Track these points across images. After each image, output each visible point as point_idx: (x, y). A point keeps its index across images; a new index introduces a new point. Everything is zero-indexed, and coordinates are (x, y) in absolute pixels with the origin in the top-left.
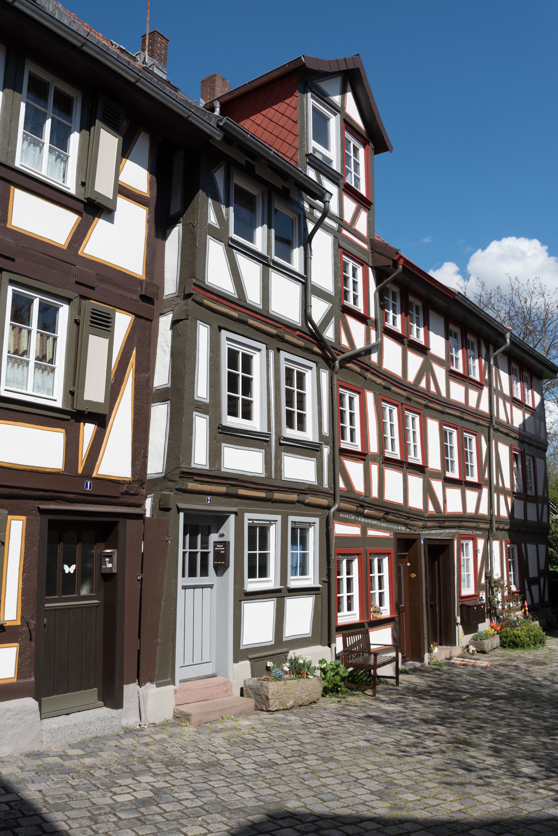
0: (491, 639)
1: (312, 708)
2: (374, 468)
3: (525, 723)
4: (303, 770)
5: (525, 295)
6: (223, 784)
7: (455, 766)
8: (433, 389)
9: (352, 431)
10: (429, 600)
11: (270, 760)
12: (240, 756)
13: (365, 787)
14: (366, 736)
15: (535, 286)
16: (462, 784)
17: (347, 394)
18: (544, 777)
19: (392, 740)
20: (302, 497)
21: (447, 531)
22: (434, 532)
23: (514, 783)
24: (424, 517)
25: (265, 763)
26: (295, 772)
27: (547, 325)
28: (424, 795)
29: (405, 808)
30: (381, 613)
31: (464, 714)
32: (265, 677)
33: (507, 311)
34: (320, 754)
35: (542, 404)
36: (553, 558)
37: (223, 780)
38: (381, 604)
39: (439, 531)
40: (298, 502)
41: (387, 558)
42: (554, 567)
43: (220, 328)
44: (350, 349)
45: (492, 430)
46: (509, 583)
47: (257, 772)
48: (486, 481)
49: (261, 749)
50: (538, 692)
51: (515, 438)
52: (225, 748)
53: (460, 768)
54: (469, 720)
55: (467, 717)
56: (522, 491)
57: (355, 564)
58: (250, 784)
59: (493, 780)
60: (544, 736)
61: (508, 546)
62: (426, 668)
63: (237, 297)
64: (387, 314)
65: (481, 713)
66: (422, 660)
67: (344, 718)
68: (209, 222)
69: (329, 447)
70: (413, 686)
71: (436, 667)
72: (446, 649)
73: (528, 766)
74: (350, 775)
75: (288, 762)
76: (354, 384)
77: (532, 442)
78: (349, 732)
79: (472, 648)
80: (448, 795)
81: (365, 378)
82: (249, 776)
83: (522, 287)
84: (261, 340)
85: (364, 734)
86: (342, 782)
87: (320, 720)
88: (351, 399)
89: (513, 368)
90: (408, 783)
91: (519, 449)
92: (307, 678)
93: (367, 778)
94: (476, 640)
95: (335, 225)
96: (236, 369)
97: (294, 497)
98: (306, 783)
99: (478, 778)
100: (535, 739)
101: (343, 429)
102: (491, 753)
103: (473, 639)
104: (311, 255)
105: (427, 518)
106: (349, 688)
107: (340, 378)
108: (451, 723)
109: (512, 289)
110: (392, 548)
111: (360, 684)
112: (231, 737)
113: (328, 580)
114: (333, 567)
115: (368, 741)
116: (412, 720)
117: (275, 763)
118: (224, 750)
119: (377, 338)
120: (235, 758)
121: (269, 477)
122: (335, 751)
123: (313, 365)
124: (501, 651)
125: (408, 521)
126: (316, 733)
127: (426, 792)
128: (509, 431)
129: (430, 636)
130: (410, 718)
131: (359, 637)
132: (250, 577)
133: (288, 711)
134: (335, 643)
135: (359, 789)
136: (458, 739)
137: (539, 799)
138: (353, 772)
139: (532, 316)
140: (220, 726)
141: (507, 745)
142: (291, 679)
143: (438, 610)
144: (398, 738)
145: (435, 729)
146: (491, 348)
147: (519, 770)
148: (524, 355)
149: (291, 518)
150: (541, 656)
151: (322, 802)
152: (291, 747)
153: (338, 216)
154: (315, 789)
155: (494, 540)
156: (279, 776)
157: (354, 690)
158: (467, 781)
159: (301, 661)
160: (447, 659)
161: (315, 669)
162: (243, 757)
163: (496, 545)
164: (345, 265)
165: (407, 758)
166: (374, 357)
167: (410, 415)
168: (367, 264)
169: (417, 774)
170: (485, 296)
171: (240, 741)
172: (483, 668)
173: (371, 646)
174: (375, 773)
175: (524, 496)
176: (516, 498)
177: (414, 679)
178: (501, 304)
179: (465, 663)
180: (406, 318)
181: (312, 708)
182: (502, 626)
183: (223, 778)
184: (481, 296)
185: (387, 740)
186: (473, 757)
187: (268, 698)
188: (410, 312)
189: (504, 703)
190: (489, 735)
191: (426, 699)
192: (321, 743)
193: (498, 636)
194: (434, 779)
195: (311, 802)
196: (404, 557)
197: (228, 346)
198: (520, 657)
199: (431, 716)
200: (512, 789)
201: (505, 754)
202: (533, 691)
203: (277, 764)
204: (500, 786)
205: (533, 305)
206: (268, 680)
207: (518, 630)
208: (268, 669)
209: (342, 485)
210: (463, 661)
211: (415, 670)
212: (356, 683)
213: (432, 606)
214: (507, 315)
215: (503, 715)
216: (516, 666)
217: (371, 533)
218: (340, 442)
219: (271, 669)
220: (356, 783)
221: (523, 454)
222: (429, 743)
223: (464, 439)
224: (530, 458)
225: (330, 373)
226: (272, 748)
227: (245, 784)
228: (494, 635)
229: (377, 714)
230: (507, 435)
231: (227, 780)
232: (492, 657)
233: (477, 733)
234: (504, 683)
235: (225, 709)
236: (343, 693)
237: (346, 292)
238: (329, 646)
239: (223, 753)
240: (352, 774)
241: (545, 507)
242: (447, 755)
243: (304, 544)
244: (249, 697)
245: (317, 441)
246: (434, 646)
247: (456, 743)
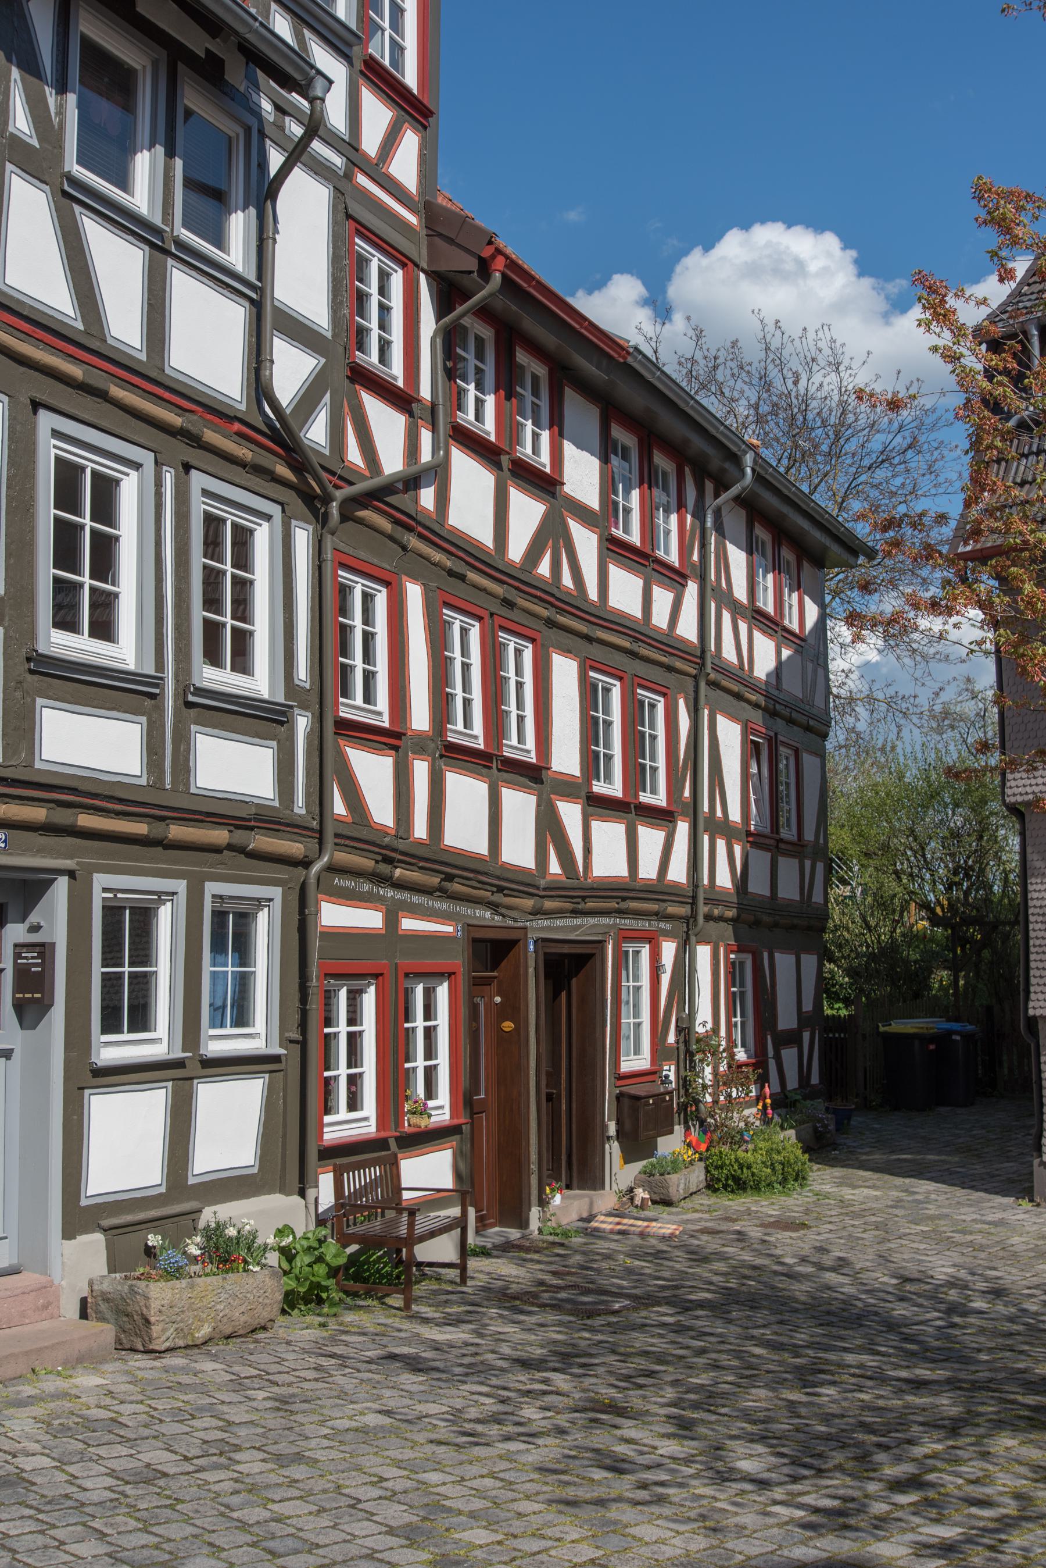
0: (685, 1171)
1: (256, 1341)
2: (421, 769)
3: (752, 1360)
4: (228, 1486)
5: (795, 364)
6: (33, 1526)
7: (586, 1463)
8: (567, 580)
9: (369, 678)
10: (544, 1083)
11: (148, 1465)
12: (75, 1459)
13: (374, 1518)
14: (384, 1401)
15: (820, 344)
16: (601, 1502)
17: (359, 587)
18: (787, 1479)
19: (445, 1409)
20: (240, 837)
21: (592, 921)
22: (559, 923)
23: (718, 1495)
24: (538, 888)
25: (136, 1474)
26: (209, 1490)
27: (842, 441)
28: (512, 1530)
29: (465, 1561)
30: (430, 1116)
31: (614, 1344)
32: (142, 1270)
33: (752, 402)
34: (270, 1448)
35: (821, 626)
36: (834, 986)
37: (30, 1517)
38: (430, 1091)
39: (571, 922)
40: (230, 847)
41: (446, 985)
42: (836, 1006)
43: (36, 405)
44: (367, 474)
45: (703, 685)
46: (731, 1044)
47: (117, 1496)
48: (685, 805)
49: (129, 1440)
50: (784, 1289)
51: (756, 706)
52: (38, 1441)
53: (599, 1467)
54: (625, 1357)
55: (622, 1350)
56: (767, 831)
57: (369, 1000)
58: (97, 1524)
59: (671, 1491)
60: (792, 1388)
61: (732, 956)
62: (532, 1241)
63: (82, 328)
64: (461, 393)
65: (654, 1341)
66: (523, 1223)
67: (333, 1361)
68: (11, 129)
69: (309, 714)
70: (500, 1283)
71: (557, 1239)
72: (581, 1197)
73: (751, 1456)
74: (340, 1493)
75: (192, 1468)
76: (375, 561)
77: (794, 715)
78: (343, 1394)
79: (641, 1194)
80: (567, 1529)
81: (404, 548)
82: (95, 1505)
83: (789, 344)
84: (141, 441)
85: (379, 1397)
86: (322, 1510)
87: (274, 1368)
88: (368, 598)
89: (757, 537)
90: (478, 1504)
91: (764, 730)
92: (245, 1271)
93: (380, 1498)
94: (651, 1175)
95: (337, 161)
96: (77, 511)
97: (220, 836)
98: (235, 1515)
99: (639, 1488)
100: (771, 1394)
101: (346, 671)
102: (671, 1430)
103: (645, 1173)
104: (276, 231)
105: (545, 889)
106: (347, 1293)
107: (342, 546)
108: (583, 1366)
109: (767, 349)
110: (458, 960)
111: (374, 1283)
112: (54, 1415)
113: (301, 1038)
114: (315, 1005)
115: (388, 1413)
116: (493, 1363)
117: (160, 1472)
118: (37, 1447)
119: (434, 452)
120: (62, 1463)
121: (157, 785)
122: (307, 1438)
123: (275, 510)
124: (705, 1200)
125: (498, 898)
126: (264, 1399)
127: (517, 1523)
128: (743, 689)
129: (545, 1167)
130: (490, 1356)
131: (375, 1172)
132: (105, 1030)
133: (197, 1351)
134: (317, 1187)
135: (360, 1524)
136: (597, 1401)
137: (772, 1527)
138: (347, 1487)
139: (810, 416)
140: (27, 1390)
141: (709, 1411)
142: (207, 1275)
143: (564, 1107)
144: (458, 1403)
145: (545, 1381)
146: (709, 486)
147: (731, 1465)
148: (786, 509)
149: (212, 888)
150: (797, 1209)
151: (270, 1557)
152: (201, 1434)
153: (346, 138)
154: (255, 1529)
155: (699, 942)
156: (169, 1502)
157: (359, 1296)
158: (612, 1496)
159: (231, 1232)
160: (581, 1220)
161: (265, 1250)
162: (81, 1460)
163: (703, 954)
164: (362, 263)
165: (477, 1448)
166: (427, 497)
167: (512, 643)
168: (417, 265)
169: (499, 1484)
170: (702, 362)
171: (77, 1424)
172: (663, 1238)
173: (404, 1192)
174: (399, 1485)
175: (773, 842)
176: (754, 844)
177: (505, 1268)
178: (740, 385)
179: (624, 1228)
180: (508, 403)
181: (256, 1341)
182: (711, 1142)
183: (32, 1512)
184: (693, 361)
185: (433, 1408)
186: (628, 1441)
187: (147, 1322)
188: (518, 389)
189: (707, 1316)
190: (669, 1389)
191: (529, 1313)
192: (274, 1421)
193: (702, 1164)
194: (538, 1493)
195: (245, 1559)
196: (487, 982)
197: (54, 451)
198: (748, 1212)
199: (539, 1351)
200: (714, 1509)
201: (702, 1430)
202: (773, 1288)
203: (165, 1475)
204: (687, 1503)
205: (812, 389)
206: (148, 1277)
207: (747, 1151)
208: (149, 1251)
209: (339, 807)
210: (618, 1224)
211: (506, 1248)
212: (365, 1280)
213: (550, 1098)
214: (752, 411)
215: (703, 1344)
216: (739, 1233)
217: (408, 924)
218: (337, 703)
219: (158, 1252)
220: (353, 1511)
221: (773, 742)
222: (530, 1412)
223: (637, 705)
224: (789, 752)
225: (315, 531)
226: (155, 1437)
227: (84, 1524)
228: (691, 1163)
229: (412, 1351)
230: (738, 696)
231: (40, 1516)
232: (686, 1213)
233: (641, 1387)
234: (711, 1271)
235: (40, 1350)
236: (333, 1304)
237: (362, 333)
238: (302, 1194)
239: (33, 1455)
240: (346, 1491)
241: (820, 867)
242: (569, 1438)
243: (244, 951)
244: (102, 1319)
245: (281, 699)
246: (552, 1190)
247: (593, 1410)
